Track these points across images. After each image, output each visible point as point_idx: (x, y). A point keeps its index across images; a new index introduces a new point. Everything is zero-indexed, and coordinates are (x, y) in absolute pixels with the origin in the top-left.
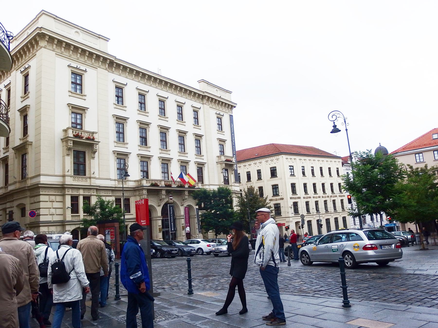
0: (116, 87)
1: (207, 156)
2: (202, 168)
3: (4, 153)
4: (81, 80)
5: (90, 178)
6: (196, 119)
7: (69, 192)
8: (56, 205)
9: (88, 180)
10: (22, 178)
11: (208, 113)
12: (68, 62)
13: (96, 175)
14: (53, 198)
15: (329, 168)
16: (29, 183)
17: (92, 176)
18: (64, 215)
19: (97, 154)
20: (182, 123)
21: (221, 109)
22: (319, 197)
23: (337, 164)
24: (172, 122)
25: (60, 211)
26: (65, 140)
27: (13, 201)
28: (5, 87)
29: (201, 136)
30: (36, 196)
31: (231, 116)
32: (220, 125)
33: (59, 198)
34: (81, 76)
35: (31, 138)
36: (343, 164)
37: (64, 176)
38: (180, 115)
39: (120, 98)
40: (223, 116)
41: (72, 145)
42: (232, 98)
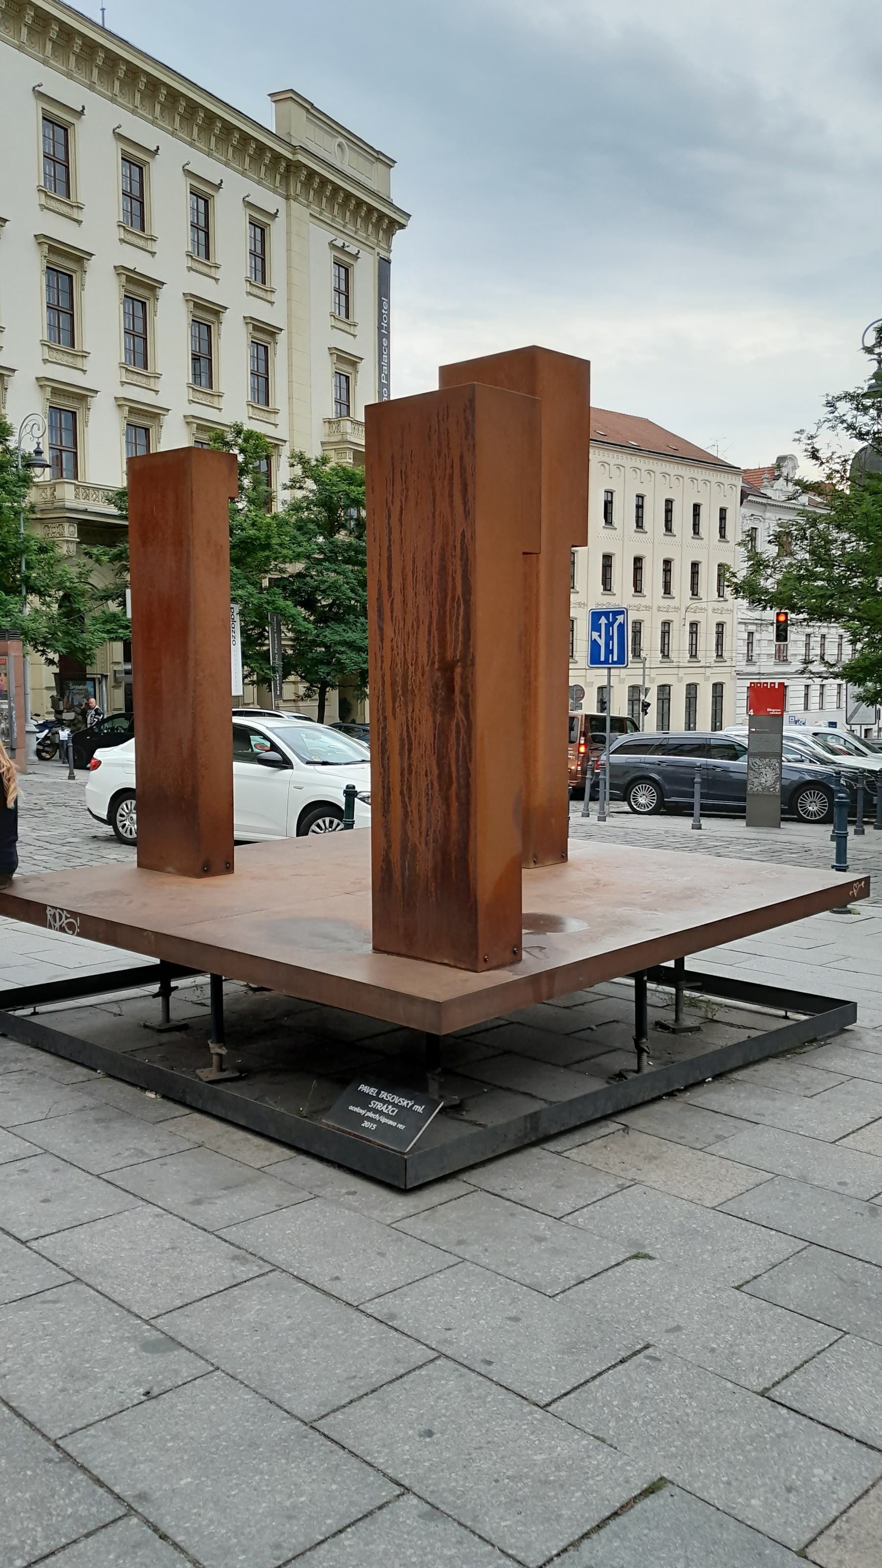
0: (47, 118)
1: (291, 414)
6: (260, 257)
11: (306, 239)
15: (669, 502)
20: (205, 269)
21: (350, 229)
22: (648, 608)
23: (721, 493)
24: (168, 259)
29: (272, 332)
31: (384, 264)
32: (344, 292)
36: (744, 495)
38: (136, 200)
39: (59, 167)
40: (356, 257)
41: (351, 461)
42: (401, 191)
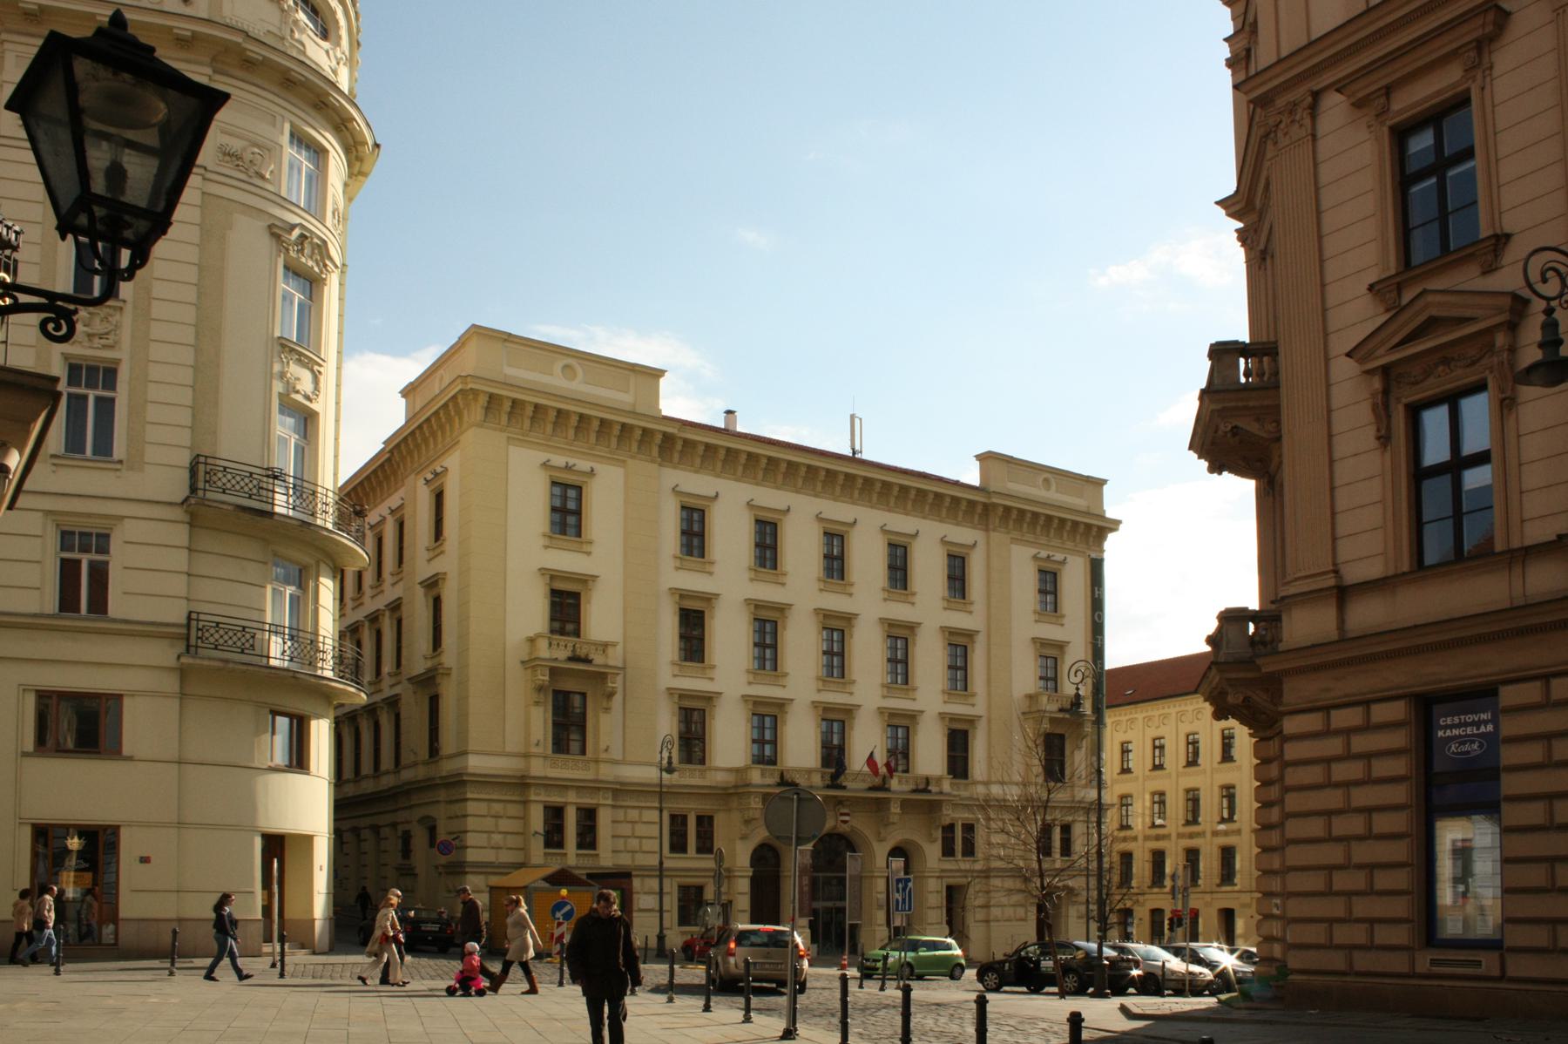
2: (965, 733)
3: (392, 686)
4: (579, 499)
5: (597, 761)
7: (539, 798)
8: (505, 825)
9: (592, 765)
10: (431, 756)
12: (543, 456)
13: (616, 754)
14: (497, 807)
16: (447, 767)
17: (603, 756)
18: (524, 849)
19: (618, 698)
25: (512, 841)
26: (530, 664)
27: (411, 807)
28: (392, 512)
30: (457, 801)
33: (513, 810)
34: (579, 489)
35: (448, 658)
37: (526, 756)
40: (1064, 562)
